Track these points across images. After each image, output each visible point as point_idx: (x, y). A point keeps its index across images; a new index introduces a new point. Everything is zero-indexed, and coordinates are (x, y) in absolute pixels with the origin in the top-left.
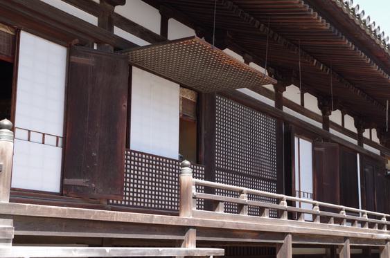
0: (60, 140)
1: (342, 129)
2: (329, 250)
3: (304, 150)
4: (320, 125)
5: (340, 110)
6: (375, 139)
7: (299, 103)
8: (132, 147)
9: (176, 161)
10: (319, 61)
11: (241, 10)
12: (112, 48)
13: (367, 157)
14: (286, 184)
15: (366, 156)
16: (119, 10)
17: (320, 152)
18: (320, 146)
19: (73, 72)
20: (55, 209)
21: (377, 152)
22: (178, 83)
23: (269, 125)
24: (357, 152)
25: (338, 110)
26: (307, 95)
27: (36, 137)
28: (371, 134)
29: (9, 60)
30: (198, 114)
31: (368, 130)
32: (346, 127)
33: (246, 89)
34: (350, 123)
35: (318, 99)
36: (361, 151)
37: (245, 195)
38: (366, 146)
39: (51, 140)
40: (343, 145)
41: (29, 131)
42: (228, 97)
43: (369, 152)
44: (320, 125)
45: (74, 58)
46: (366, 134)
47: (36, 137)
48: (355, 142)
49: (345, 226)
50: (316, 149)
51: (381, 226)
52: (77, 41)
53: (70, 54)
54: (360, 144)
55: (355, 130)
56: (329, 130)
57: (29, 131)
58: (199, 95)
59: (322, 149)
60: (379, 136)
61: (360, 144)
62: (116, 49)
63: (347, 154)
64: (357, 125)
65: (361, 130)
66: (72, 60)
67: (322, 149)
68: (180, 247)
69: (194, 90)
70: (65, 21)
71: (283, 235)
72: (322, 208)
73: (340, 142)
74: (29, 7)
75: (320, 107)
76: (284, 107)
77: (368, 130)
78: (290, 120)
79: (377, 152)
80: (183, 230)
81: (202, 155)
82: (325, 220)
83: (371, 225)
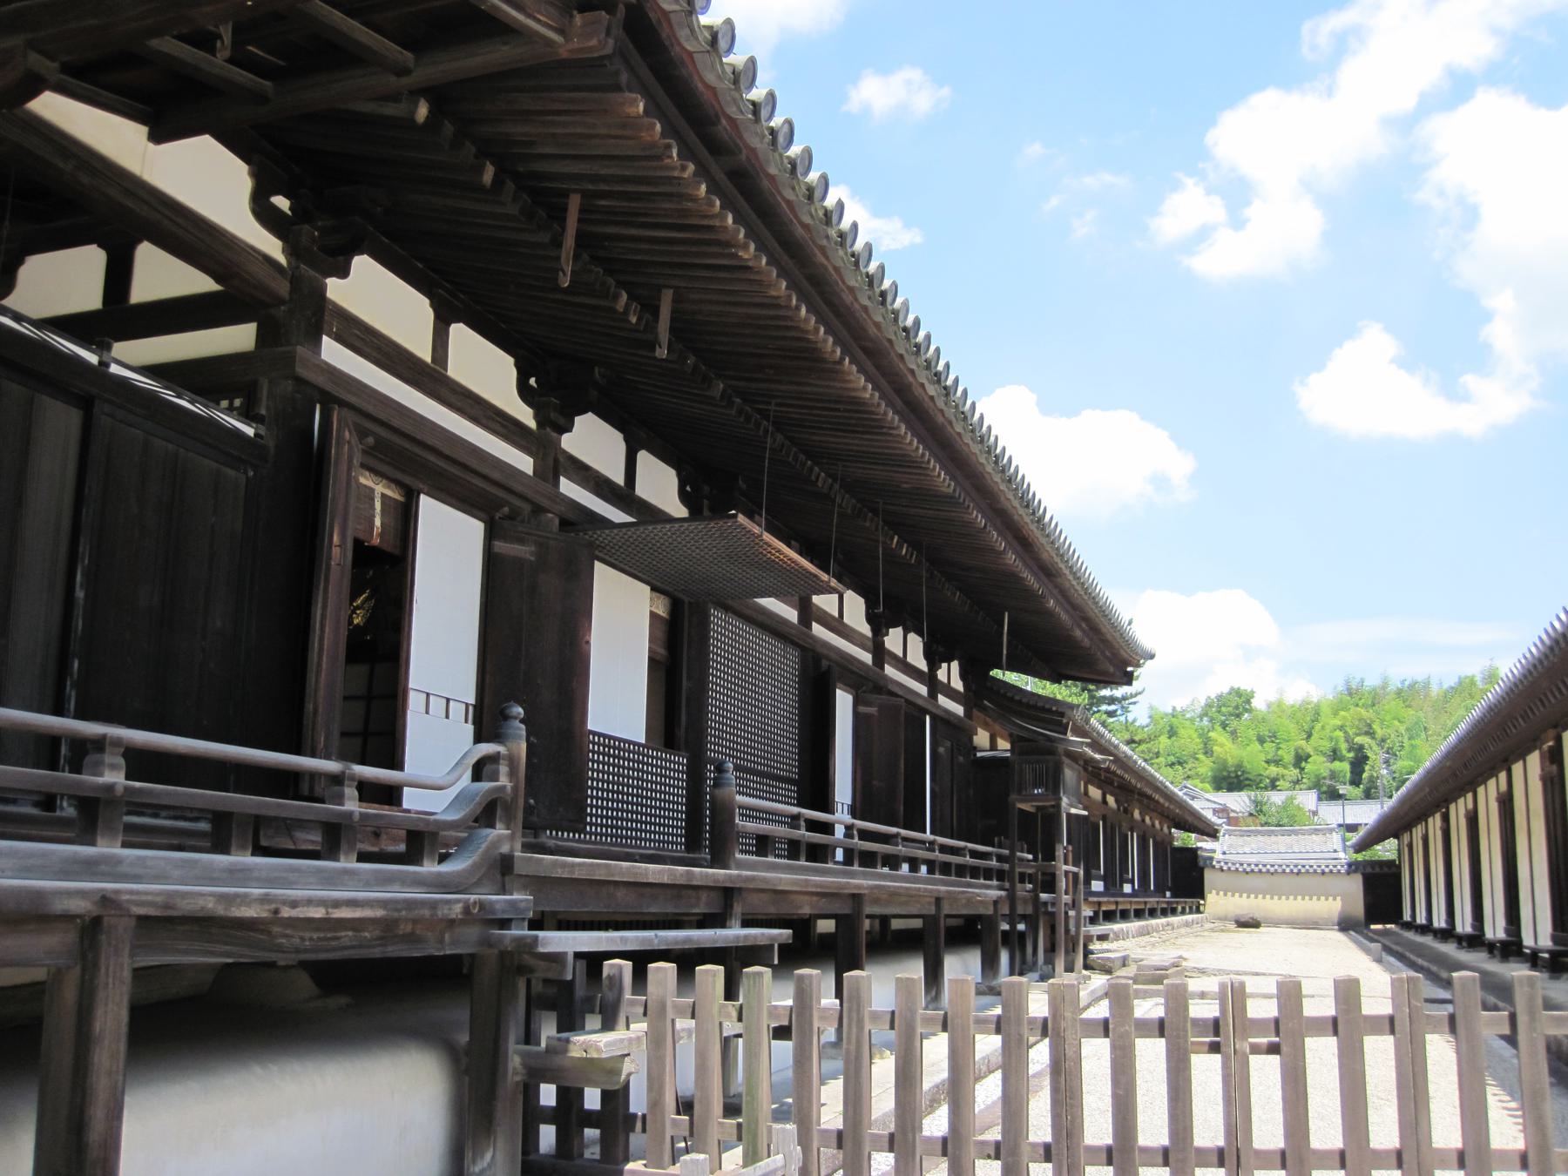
1: (836, 625)
2: (877, 922)
3: (844, 702)
4: (867, 657)
6: (958, 684)
7: (836, 614)
9: (639, 745)
10: (902, 540)
13: (944, 722)
14: (816, 790)
15: (942, 719)
16: (335, 289)
17: (868, 716)
19: (492, 565)
20: (579, 864)
21: (958, 709)
22: (647, 583)
23: (787, 663)
24: (924, 711)
25: (579, 420)
27: (437, 705)
29: (397, 552)
32: (909, 659)
35: (679, 475)
36: (934, 710)
39: (457, 710)
42: (727, 609)
43: (947, 711)
44: (923, 690)
45: (500, 546)
47: (437, 705)
48: (524, 463)
50: (862, 709)
54: (933, 695)
56: (557, 484)
58: (676, 606)
59: (873, 710)
60: (963, 676)
61: (933, 695)
62: (565, 524)
63: (913, 713)
64: (870, 618)
66: (496, 550)
67: (873, 710)
68: (723, 926)
70: (496, 476)
73: (909, 697)
75: (684, 497)
76: (325, 338)
78: (825, 652)
79: (958, 709)
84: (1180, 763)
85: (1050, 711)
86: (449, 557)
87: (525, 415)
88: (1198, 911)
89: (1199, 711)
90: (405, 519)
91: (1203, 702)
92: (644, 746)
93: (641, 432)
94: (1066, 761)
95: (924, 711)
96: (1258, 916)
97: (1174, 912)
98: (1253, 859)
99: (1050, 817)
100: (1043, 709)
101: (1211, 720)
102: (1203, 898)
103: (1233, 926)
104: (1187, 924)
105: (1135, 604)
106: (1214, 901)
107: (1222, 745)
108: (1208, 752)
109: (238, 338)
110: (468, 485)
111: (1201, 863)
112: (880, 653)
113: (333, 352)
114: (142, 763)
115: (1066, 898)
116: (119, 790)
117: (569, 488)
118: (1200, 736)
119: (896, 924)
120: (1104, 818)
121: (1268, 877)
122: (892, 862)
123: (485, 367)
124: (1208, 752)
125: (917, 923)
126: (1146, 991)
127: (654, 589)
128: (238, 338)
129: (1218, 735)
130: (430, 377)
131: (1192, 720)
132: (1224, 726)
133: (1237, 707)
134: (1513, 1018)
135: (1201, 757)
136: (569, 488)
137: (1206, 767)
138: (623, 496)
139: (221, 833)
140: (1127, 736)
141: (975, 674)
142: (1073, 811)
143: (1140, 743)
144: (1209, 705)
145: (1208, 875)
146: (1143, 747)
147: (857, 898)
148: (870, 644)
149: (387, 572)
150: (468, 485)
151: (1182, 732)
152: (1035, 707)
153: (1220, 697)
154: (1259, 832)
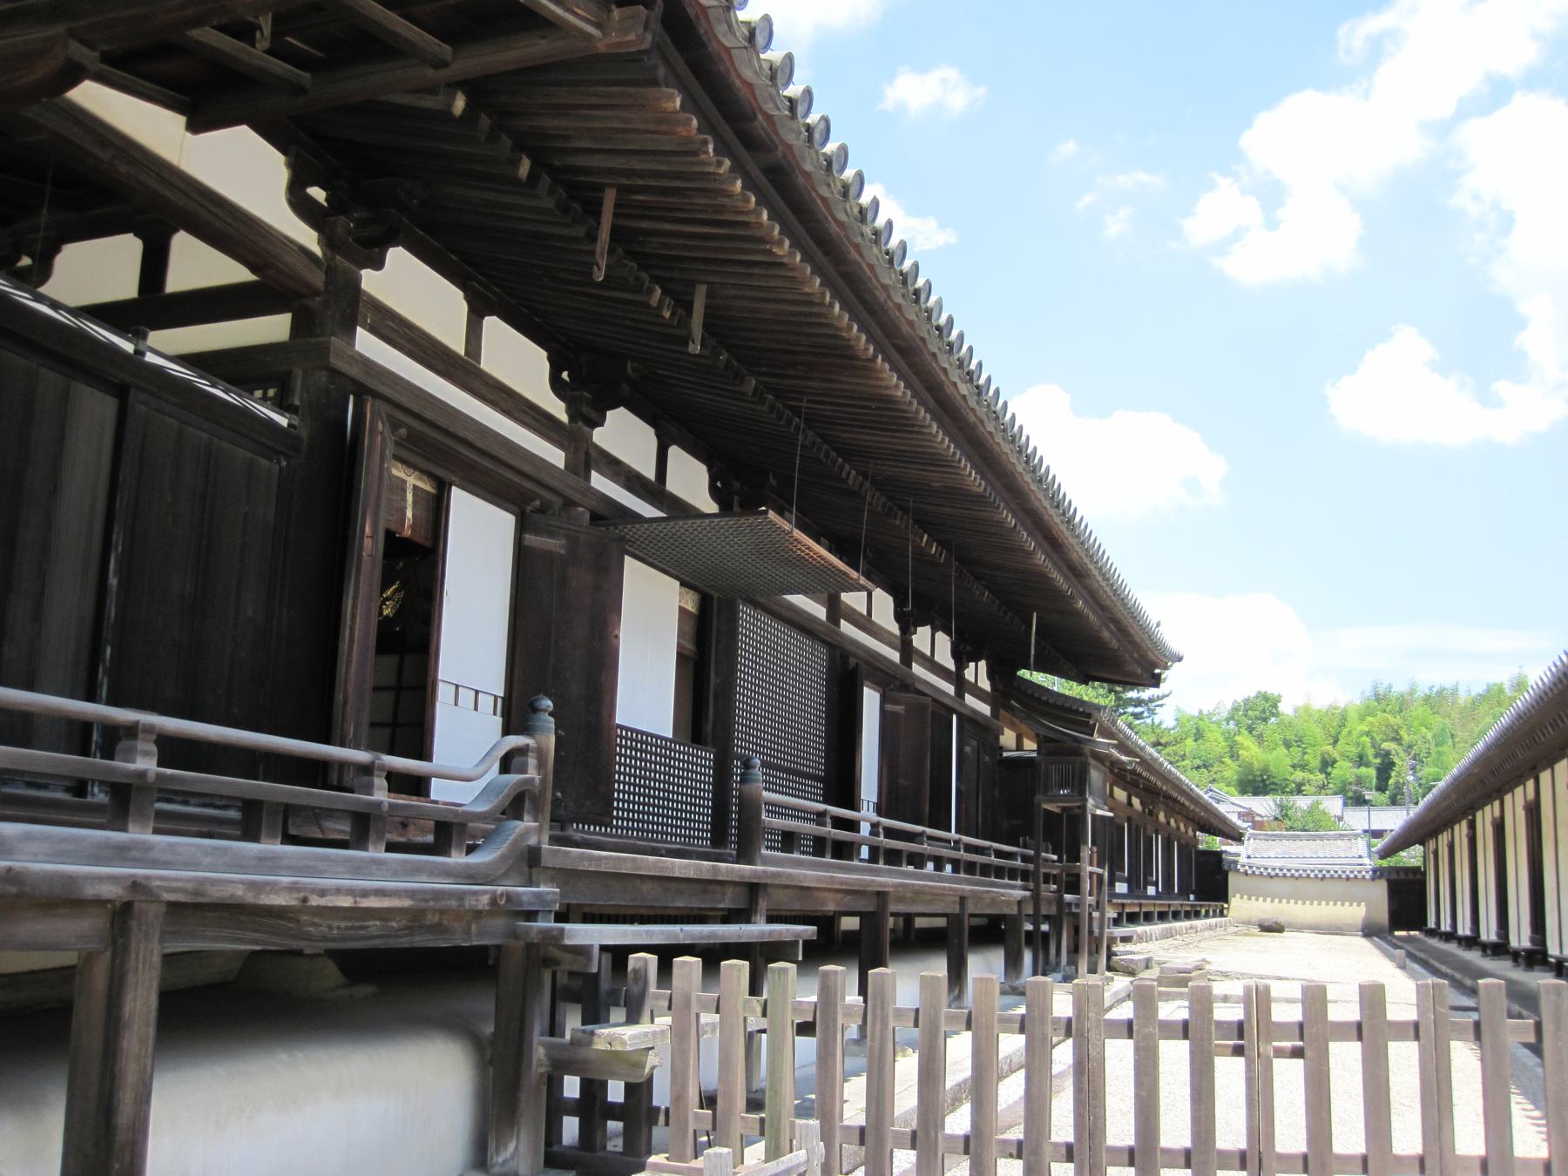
0: (500, 702)
2: (901, 920)
3: (871, 700)
5: (394, 242)
6: (985, 684)
9: (667, 739)
10: (932, 538)
11: (826, 447)
12: (587, 516)
13: (970, 722)
14: (842, 788)
16: (370, 281)
17: (895, 715)
18: (896, 702)
19: (523, 559)
21: (986, 709)
22: (676, 578)
26: (493, 325)
27: (467, 697)
28: (978, 673)
32: (672, 486)
33: (647, 515)
35: (710, 471)
37: (380, 782)
39: (486, 703)
41: (477, 692)
42: (756, 605)
44: (950, 689)
47: (467, 697)
49: (881, 865)
50: (889, 707)
52: (537, 503)
53: (521, 528)
54: (960, 695)
55: (950, 664)
57: (477, 692)
58: (705, 602)
59: (899, 708)
60: (991, 676)
61: (960, 695)
62: (596, 518)
63: (940, 712)
64: (899, 616)
67: (899, 708)
69: (824, 642)
72: (891, 833)
73: (937, 696)
74: (479, 444)
75: (715, 492)
78: (853, 649)
81: (709, 727)
84: (1205, 766)
85: (1077, 712)
86: (479, 550)
87: (557, 409)
88: (1222, 914)
89: (1225, 715)
90: (436, 511)
91: (1229, 707)
92: (671, 741)
93: (672, 427)
94: (1092, 762)
95: (952, 711)
96: (1282, 920)
97: (1197, 915)
98: (1277, 863)
99: (1076, 818)
100: (1070, 710)
101: (1238, 724)
102: (1227, 901)
103: (1256, 930)
104: (1210, 928)
105: (1157, 596)
106: (1238, 905)
107: (1248, 749)
108: (1234, 756)
109: (272, 328)
110: (502, 479)
111: (1226, 867)
112: (587, 458)
113: (367, 343)
114: (174, 751)
116: (151, 777)
118: (1226, 739)
119: (920, 923)
120: (1129, 820)
121: (1293, 882)
122: (917, 860)
123: (517, 359)
124: (1234, 756)
125: (941, 922)
126: (1168, 994)
127: (683, 584)
128: (272, 328)
129: (1245, 740)
131: (1218, 723)
132: (1250, 729)
133: (1263, 711)
135: (1227, 760)
137: (1231, 770)
138: (654, 490)
139: (250, 821)
140: (1153, 739)
142: (1099, 812)
143: (1165, 745)
144: (1236, 709)
145: (1233, 879)
146: (1169, 749)
147: (881, 896)
148: (898, 642)
150: (502, 479)
151: (1208, 735)
152: (1062, 708)
153: (1246, 701)
154: (1285, 837)
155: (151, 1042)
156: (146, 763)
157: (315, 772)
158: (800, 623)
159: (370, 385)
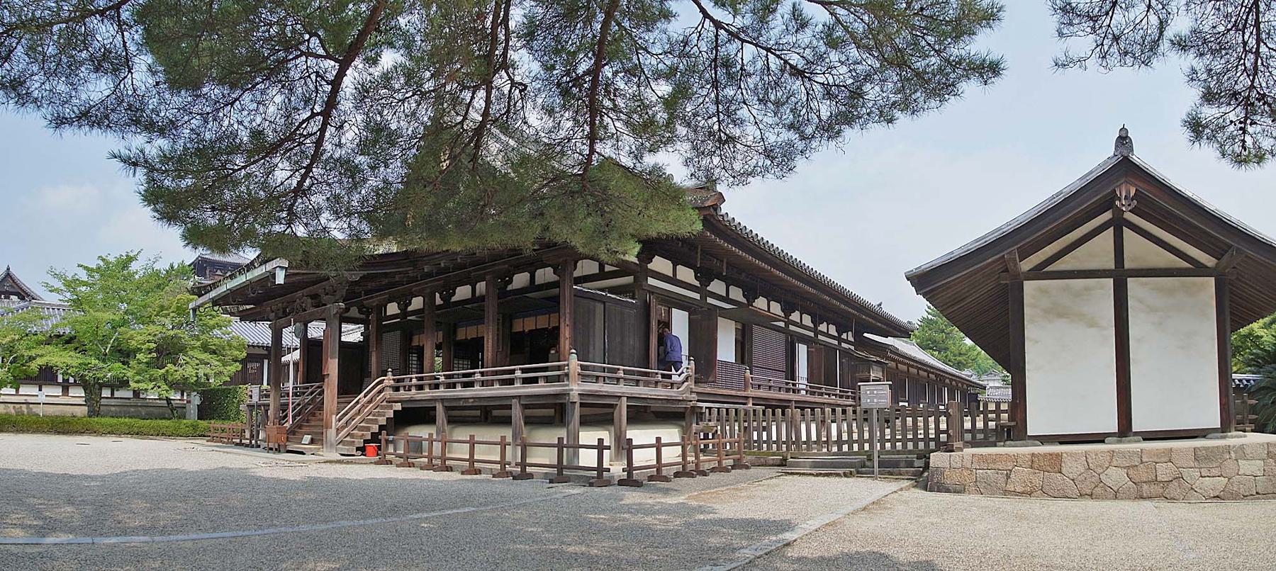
1: (801, 326)
3: (802, 350)
4: (812, 334)
8: (1211, 281)
13: (845, 353)
14: (791, 373)
30: (743, 337)
31: (678, 440)
34: (833, 330)
38: (843, 345)
40: (826, 345)
44: (812, 334)
46: (844, 336)
51: (848, 397)
54: (816, 335)
57: (1125, 428)
58: (744, 326)
61: (816, 335)
63: (832, 349)
65: (840, 335)
71: (790, 401)
77: (678, 440)
80: (747, 398)
82: (813, 393)
83: (841, 397)
86: (680, 323)
87: (697, 283)
90: (669, 314)
93: (729, 282)
109: (629, 280)
110: (683, 304)
112: (817, 332)
113: (651, 281)
114: (625, 372)
115: (1232, 128)
117: (710, 300)
122: (821, 394)
123: (686, 274)
128: (629, 280)
130: (672, 280)
134: (1099, 439)
136: (710, 300)
138: (726, 299)
139: (637, 383)
141: (858, 335)
149: (666, 324)
150: (683, 304)
155: (227, 424)
156: (621, 374)
157: (646, 374)
158: (778, 329)
159: (653, 291)
